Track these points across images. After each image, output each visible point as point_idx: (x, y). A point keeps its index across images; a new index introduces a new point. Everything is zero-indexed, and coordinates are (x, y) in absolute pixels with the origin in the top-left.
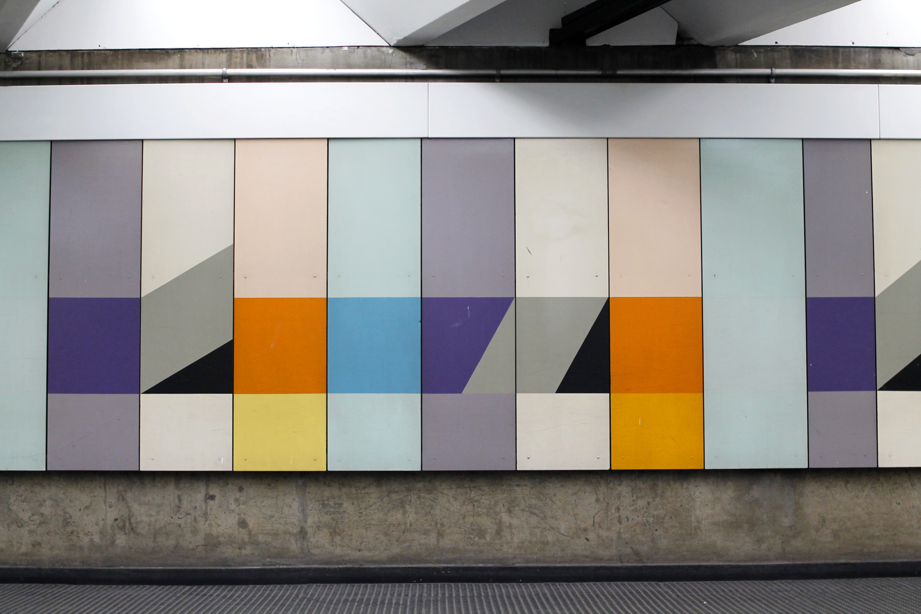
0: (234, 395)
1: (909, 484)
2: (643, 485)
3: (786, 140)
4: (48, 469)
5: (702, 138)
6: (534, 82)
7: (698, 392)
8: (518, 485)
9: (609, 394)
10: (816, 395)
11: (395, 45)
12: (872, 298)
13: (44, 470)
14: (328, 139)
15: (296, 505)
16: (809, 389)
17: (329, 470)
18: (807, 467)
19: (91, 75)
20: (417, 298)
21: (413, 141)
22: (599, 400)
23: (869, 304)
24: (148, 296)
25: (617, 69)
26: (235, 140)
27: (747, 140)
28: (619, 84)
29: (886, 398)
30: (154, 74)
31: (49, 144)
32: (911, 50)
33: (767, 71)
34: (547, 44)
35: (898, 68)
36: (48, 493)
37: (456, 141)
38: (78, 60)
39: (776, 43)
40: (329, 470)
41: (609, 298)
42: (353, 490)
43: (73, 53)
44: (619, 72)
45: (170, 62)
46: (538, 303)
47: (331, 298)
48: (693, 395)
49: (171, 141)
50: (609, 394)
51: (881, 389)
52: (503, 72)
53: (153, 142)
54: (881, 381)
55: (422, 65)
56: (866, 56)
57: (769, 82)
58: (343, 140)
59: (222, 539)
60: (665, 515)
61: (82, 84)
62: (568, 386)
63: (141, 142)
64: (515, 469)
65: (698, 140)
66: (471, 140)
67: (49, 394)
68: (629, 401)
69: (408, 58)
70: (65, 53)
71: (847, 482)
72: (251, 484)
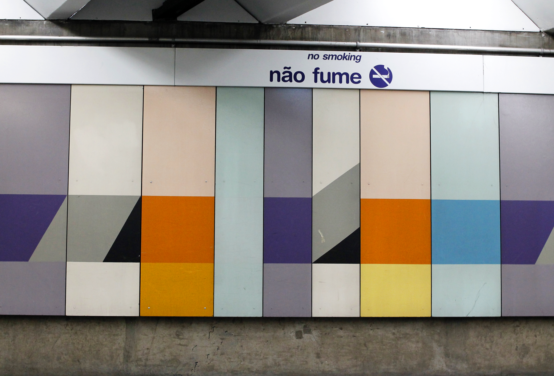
1: (45, 327)
6: (443, 53)
8: (378, 329)
9: (139, 263)
10: (271, 266)
15: (123, 336)
18: (138, 315)
22: (134, 267)
25: (159, 38)
26: (430, 91)
27: (7, 85)
28: (133, 47)
29: (318, 268)
30: (7, 39)
31: (263, 89)
32: (430, 31)
33: (354, 44)
34: (152, 20)
37: (37, 86)
39: (305, 22)
41: (141, 198)
44: (161, 40)
45: (19, 29)
47: (434, 200)
48: (204, 265)
50: (139, 263)
52: (177, 40)
54: (314, 259)
55: (65, 31)
58: (397, 91)
61: (269, 49)
63: (311, 89)
64: (64, 315)
65: (497, 94)
69: (58, 29)
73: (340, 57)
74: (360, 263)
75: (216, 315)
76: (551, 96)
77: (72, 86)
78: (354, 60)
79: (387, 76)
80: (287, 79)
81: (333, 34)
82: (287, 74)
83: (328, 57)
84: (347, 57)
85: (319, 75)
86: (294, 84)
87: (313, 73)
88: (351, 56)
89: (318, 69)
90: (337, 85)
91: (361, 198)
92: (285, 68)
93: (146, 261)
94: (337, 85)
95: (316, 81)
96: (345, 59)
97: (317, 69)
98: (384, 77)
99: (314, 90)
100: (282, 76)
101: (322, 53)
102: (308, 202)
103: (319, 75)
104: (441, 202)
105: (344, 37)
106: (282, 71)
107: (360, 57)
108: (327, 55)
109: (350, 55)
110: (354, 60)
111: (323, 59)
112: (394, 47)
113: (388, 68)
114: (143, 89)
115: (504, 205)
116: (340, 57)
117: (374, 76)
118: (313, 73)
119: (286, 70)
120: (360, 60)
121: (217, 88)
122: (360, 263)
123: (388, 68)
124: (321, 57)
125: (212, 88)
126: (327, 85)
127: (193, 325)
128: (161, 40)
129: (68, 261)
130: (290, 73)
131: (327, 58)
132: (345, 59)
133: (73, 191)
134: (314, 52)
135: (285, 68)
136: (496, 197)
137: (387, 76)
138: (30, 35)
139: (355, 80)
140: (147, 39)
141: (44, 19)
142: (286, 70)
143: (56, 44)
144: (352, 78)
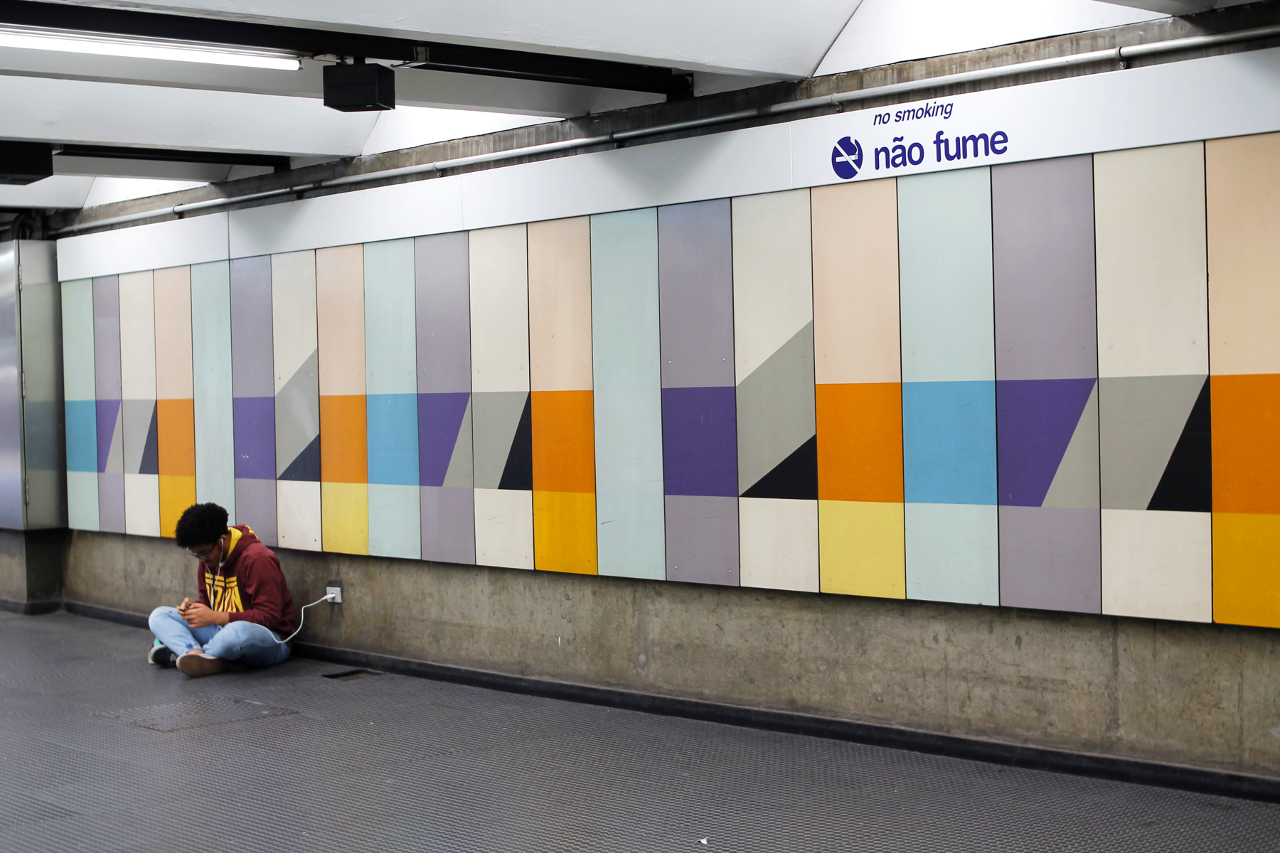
3: (1072, 158)
5: (470, 230)
7: (900, 502)
12: (187, 400)
13: (998, 605)
14: (810, 188)
16: (665, 493)
19: (1142, 52)
22: (153, 478)
23: (421, 398)
29: (280, 483)
31: (988, 170)
33: (1112, 52)
38: (1101, 42)
40: (908, 598)
41: (1209, 375)
42: (820, 616)
44: (776, 108)
46: (1130, 384)
51: (742, 496)
52: (1126, 50)
53: (916, 178)
56: (880, 74)
60: (1213, 696)
62: (1159, 502)
70: (482, 140)
72: (1061, 630)
73: (920, 113)
74: (320, 481)
75: (600, 573)
77: (1096, 157)
78: (942, 114)
79: (854, 157)
80: (898, 161)
82: (899, 152)
83: (902, 115)
84: (931, 112)
85: (942, 145)
86: (910, 169)
87: (935, 142)
88: (938, 107)
89: (941, 133)
90: (970, 161)
91: (68, 398)
92: (896, 139)
94: (970, 161)
95: (939, 159)
96: (927, 114)
97: (941, 133)
98: (851, 159)
100: (892, 155)
101: (893, 109)
103: (942, 145)
106: (890, 147)
107: (952, 105)
108: (901, 112)
109: (936, 105)
110: (942, 114)
111: (896, 121)
112: (1096, 59)
113: (856, 141)
116: (920, 113)
117: (838, 160)
118: (935, 142)
119: (898, 143)
120: (950, 112)
122: (320, 481)
123: (856, 141)
124: (893, 117)
126: (956, 163)
127: (778, 601)
128: (776, 108)
130: (902, 147)
131: (900, 117)
132: (927, 114)
134: (882, 110)
135: (896, 139)
136: (983, 372)
137: (854, 157)
139: (999, 147)
140: (311, 186)
142: (898, 143)
143: (1075, 73)
144: (993, 142)
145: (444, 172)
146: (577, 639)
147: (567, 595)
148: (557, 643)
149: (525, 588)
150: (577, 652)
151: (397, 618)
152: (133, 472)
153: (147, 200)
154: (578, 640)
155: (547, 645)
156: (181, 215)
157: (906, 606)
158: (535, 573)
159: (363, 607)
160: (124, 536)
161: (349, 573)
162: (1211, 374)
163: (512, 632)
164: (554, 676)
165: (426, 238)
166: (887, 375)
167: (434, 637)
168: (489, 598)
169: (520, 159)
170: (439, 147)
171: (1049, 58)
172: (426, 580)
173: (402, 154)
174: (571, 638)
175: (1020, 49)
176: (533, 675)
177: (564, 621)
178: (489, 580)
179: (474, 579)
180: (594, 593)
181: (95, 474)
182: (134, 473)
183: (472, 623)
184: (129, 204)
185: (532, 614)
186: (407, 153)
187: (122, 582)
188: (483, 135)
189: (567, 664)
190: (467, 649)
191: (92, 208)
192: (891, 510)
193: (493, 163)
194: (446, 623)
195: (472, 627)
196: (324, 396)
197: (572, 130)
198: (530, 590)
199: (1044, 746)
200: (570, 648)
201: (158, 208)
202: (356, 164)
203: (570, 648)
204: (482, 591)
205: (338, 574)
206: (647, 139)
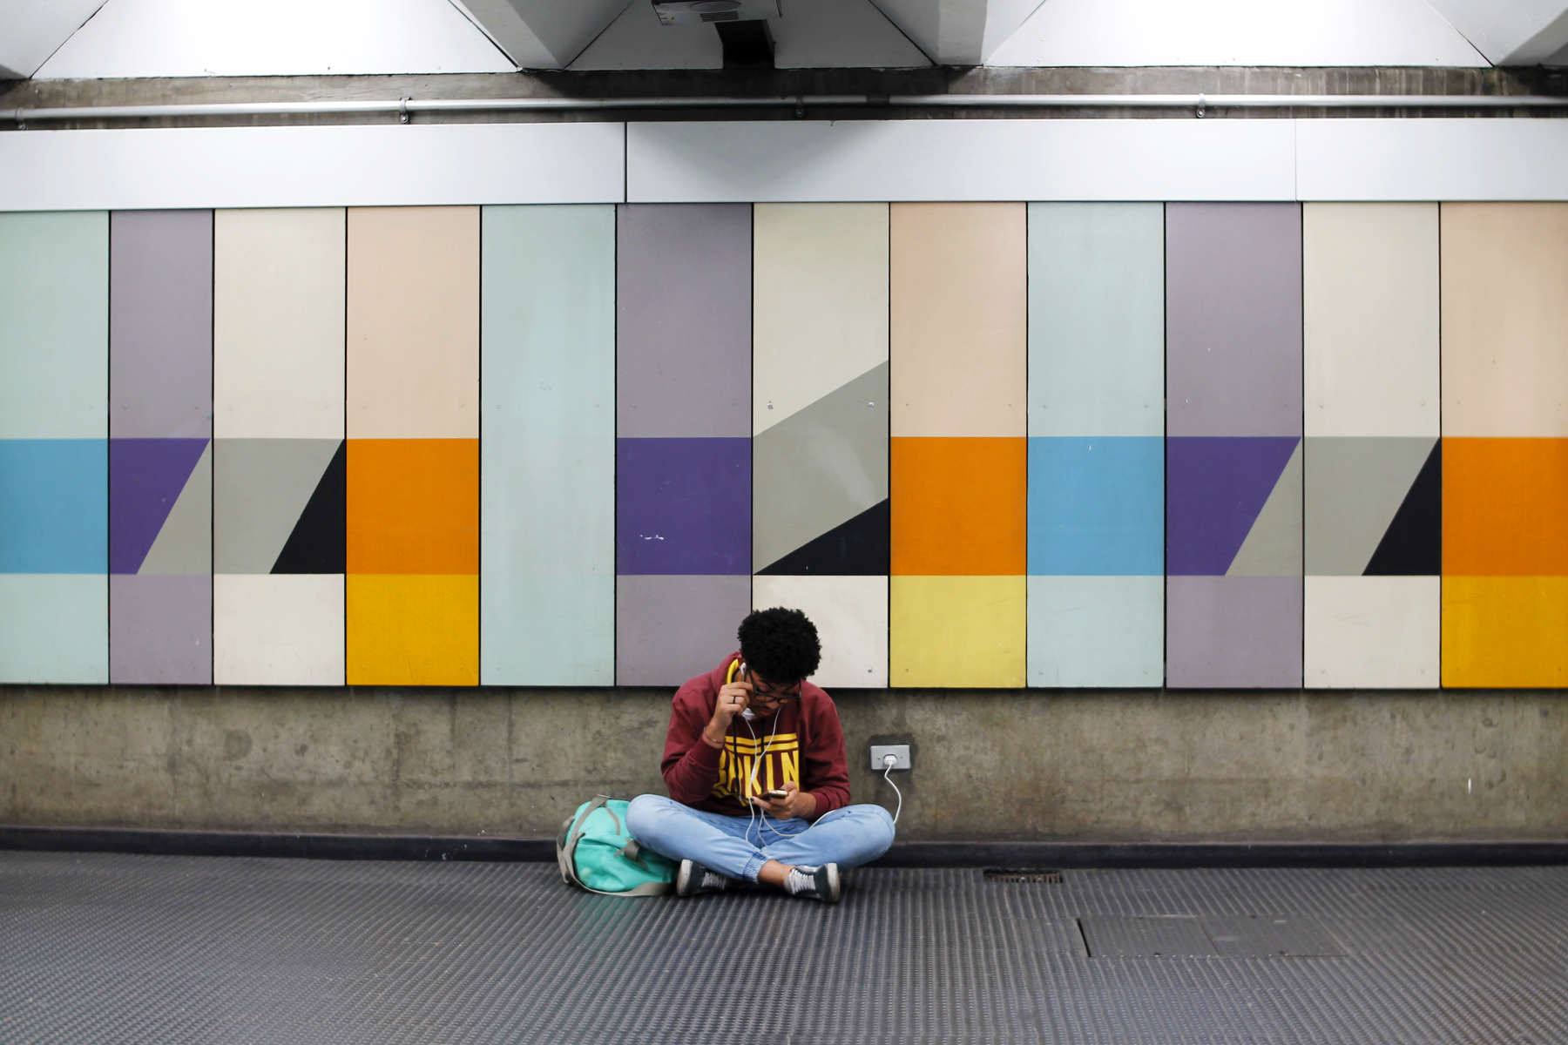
0: (892, 577)
1: (933, 707)
2: (978, 709)
4: (618, 684)
5: (1306, 202)
11: (1533, 57)
12: (746, 439)
17: (892, 686)
20: (1156, 438)
21: (604, 207)
22: (331, 583)
24: (764, 434)
25: (889, 95)
29: (759, 580)
35: (90, 104)
36: (108, 711)
37: (1232, 206)
41: (1440, 441)
43: (1030, 72)
44: (894, 100)
46: (1336, 445)
47: (352, 440)
49: (1071, 204)
51: (756, 574)
52: (808, 100)
57: (1392, 116)
59: (543, 784)
62: (1383, 563)
65: (1162, 205)
66: (1222, 206)
67: (618, 577)
68: (1463, 585)
71: (87, 696)
74: (344, 572)
76: (1196, 204)
81: (1129, 78)
91: (892, 436)
93: (361, 570)
99: (1305, 206)
102: (745, 447)
104: (1457, 441)
105: (1378, 85)
114: (616, 211)
115: (115, 448)
121: (484, 208)
122: (344, 572)
125: (474, 208)
128: (894, 100)
129: (1319, 572)
133: (1314, 429)
136: (1154, 429)
138: (447, 98)
140: (862, 99)
141: (1490, 66)
145: (1211, 111)
146: (1507, 778)
147: (1487, 719)
148: (1464, 789)
149: (1393, 716)
150: (1507, 797)
151: (1068, 781)
152: (1335, 569)
153: (252, 82)
154: (1509, 780)
155: (1442, 794)
156: (411, 116)
157: (1028, 692)
158: (1444, 692)
159: (973, 772)
160: (207, 693)
161: (919, 718)
162: (348, 437)
163: (1364, 782)
164: (1550, 835)
165: (964, 205)
166: (1011, 428)
167: (1168, 804)
168: (1309, 736)
169: (1389, 111)
170: (1194, 74)
171: (1350, 94)
172: (1150, 721)
173: (1097, 75)
174: (1495, 779)
175: (1266, 75)
176: (1409, 838)
177: (1480, 758)
178: (1310, 710)
179: (1271, 710)
180: (1545, 714)
181: (98, 582)
182: (266, 573)
183: (1265, 775)
184: (106, 89)
185: (1408, 751)
186: (1107, 75)
187: (164, 778)
188: (1304, 68)
189: (1486, 816)
190: (1254, 815)
191: (68, 82)
192: (1013, 583)
193: (1325, 111)
194: (1199, 780)
195: (1266, 781)
196: (900, 439)
197: (1504, 83)
198: (1403, 718)
199: (304, 831)
200: (1492, 794)
201: (316, 98)
202: (973, 77)
203: (1492, 794)
204: (1292, 727)
205: (900, 721)
206: (1169, 112)
